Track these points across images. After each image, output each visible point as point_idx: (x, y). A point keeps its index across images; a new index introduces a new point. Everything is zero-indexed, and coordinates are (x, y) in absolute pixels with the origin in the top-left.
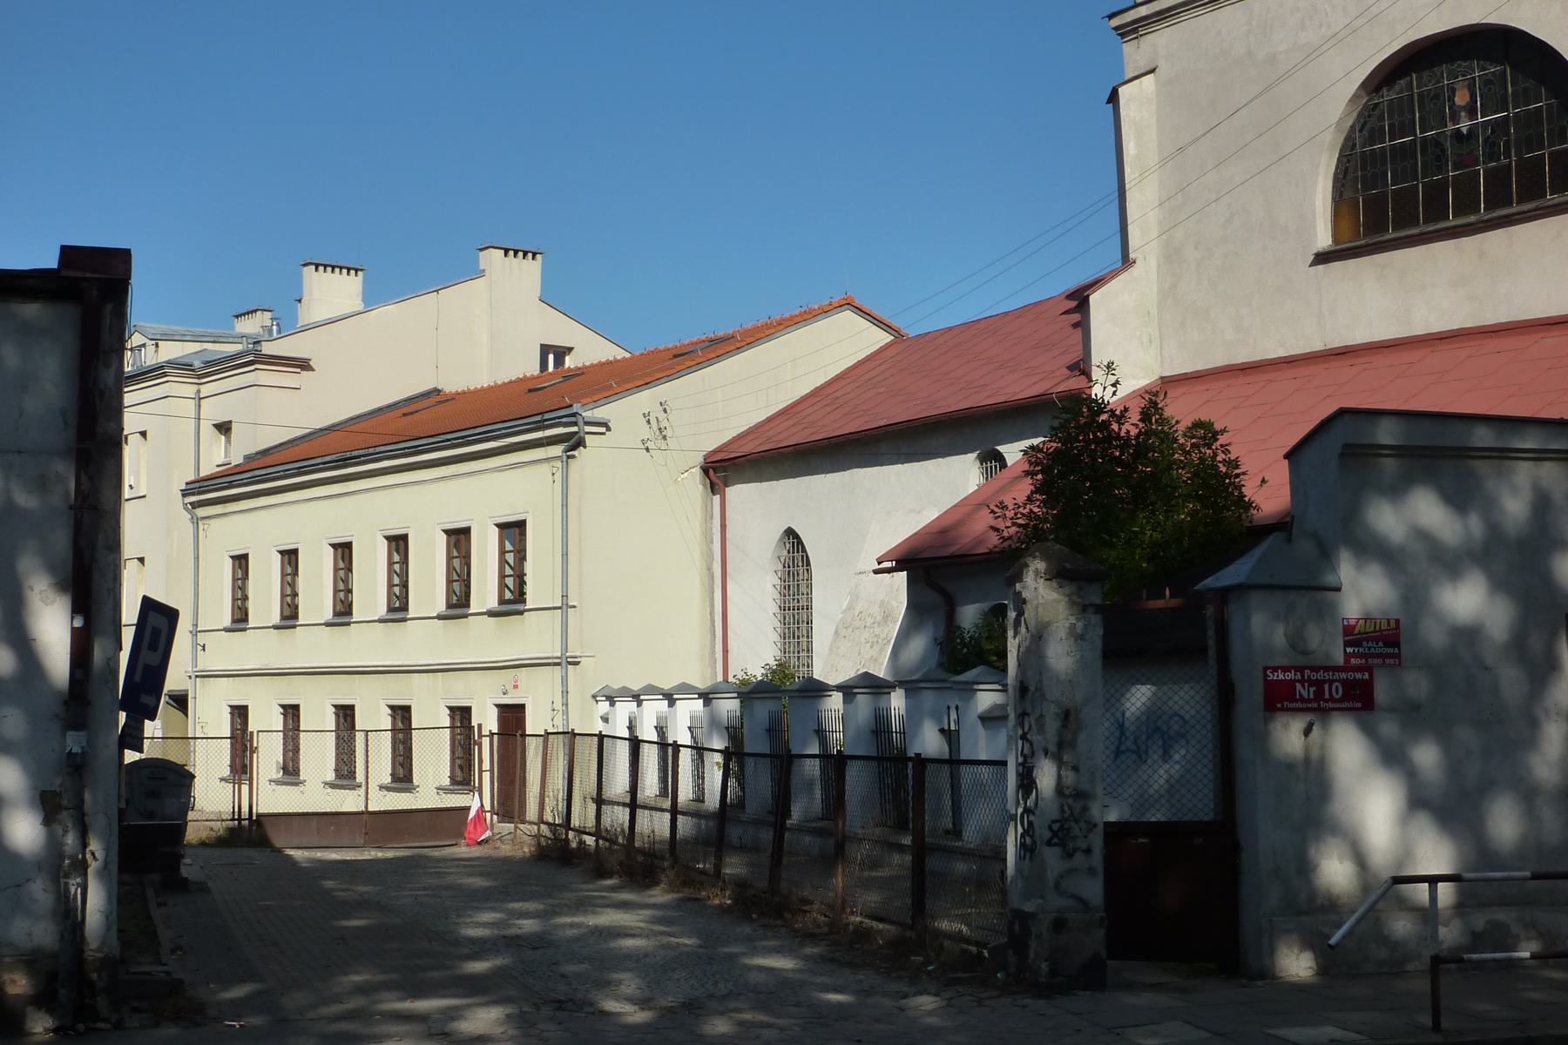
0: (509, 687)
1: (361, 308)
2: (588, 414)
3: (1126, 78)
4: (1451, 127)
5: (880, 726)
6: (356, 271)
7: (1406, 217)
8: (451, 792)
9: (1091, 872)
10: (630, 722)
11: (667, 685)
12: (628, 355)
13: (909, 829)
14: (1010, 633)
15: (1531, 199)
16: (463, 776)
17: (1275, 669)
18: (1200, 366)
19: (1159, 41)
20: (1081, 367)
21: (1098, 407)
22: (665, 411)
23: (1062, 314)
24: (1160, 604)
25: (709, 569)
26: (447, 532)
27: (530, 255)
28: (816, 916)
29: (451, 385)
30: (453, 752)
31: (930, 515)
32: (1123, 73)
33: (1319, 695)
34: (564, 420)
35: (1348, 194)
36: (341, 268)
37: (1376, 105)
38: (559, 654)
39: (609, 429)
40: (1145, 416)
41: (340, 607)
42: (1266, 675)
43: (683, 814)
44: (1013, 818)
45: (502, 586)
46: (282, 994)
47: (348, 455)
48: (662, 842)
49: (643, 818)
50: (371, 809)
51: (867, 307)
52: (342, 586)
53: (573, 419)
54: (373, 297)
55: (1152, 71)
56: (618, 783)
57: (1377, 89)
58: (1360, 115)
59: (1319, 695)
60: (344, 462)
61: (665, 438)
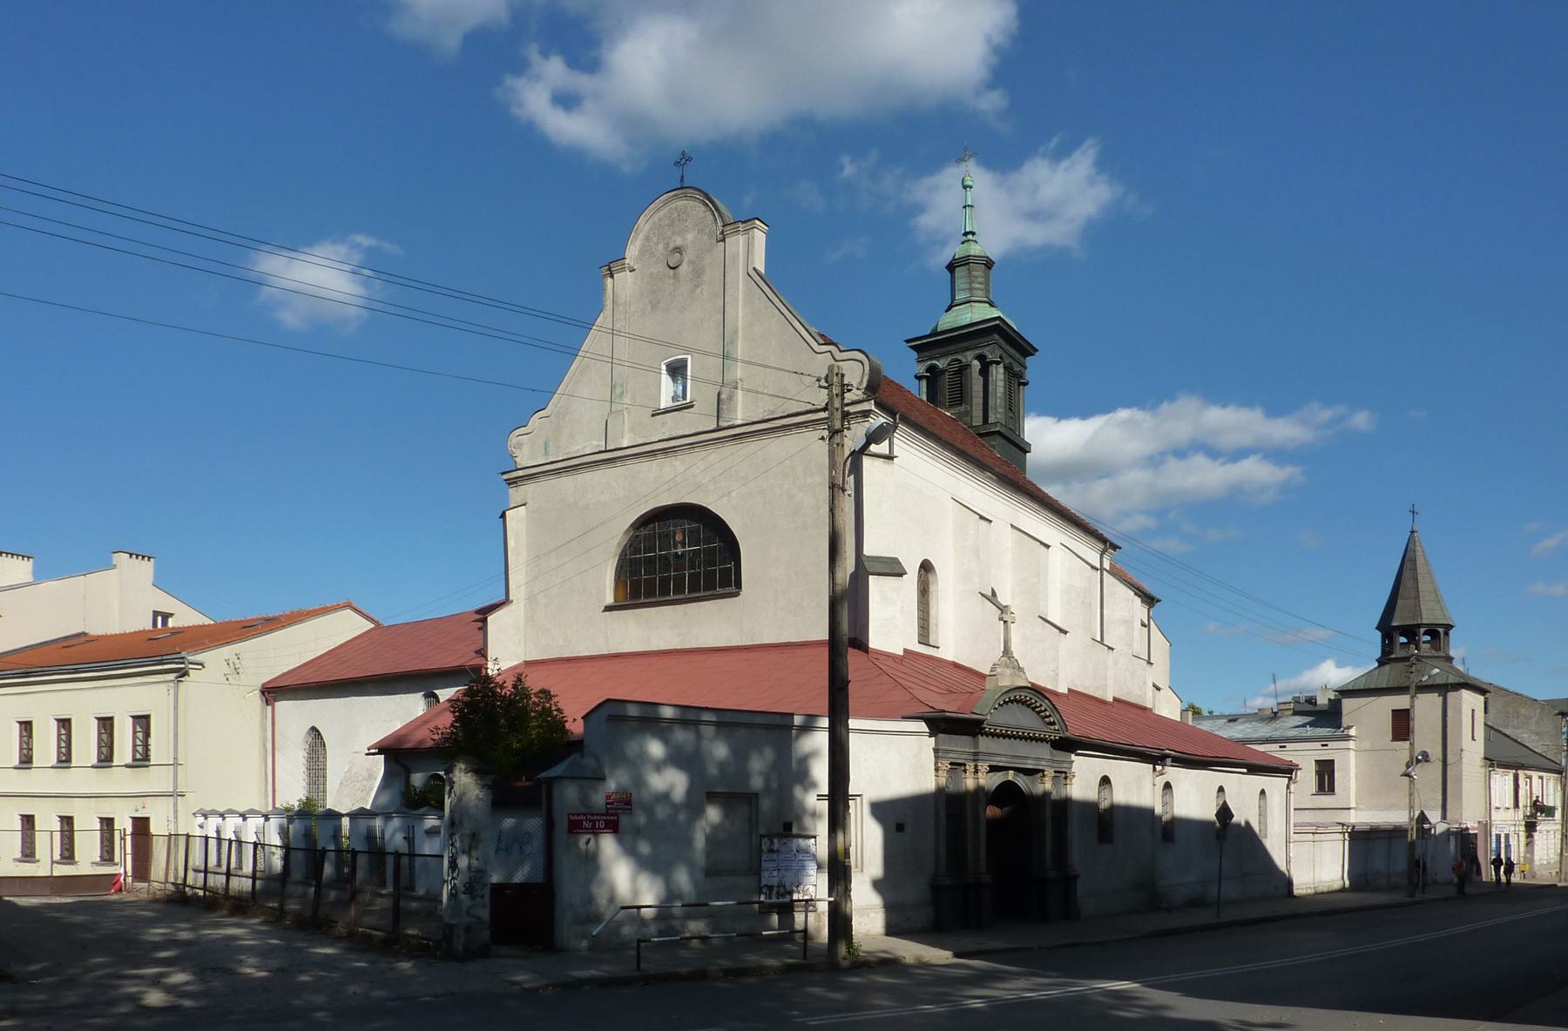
0: (140, 808)
1: (30, 578)
2: (191, 658)
3: (511, 507)
4: (673, 551)
5: (370, 836)
6: (28, 558)
7: (650, 593)
8: (102, 865)
9: (484, 906)
10: (217, 828)
11: (241, 810)
12: (212, 623)
13: (880, 810)
14: (446, 797)
15: (709, 590)
16: (107, 855)
17: (573, 815)
18: (545, 657)
19: (527, 490)
20: (483, 652)
21: (488, 679)
22: (238, 658)
23: (474, 621)
24: (519, 784)
25: (265, 746)
26: (98, 719)
27: (146, 558)
28: (341, 929)
29: (94, 630)
30: (102, 843)
31: (397, 725)
32: (508, 503)
33: (594, 827)
34: (176, 660)
35: (622, 578)
36: (18, 555)
37: (637, 536)
38: (172, 790)
39: (204, 667)
40: (515, 687)
41: (24, 758)
42: (569, 818)
43: (259, 879)
44: (445, 881)
45: (135, 751)
46: (482, 877)
47: (30, 670)
48: (248, 892)
49: (211, 878)
50: (54, 874)
51: (359, 608)
52: (25, 746)
53: (182, 660)
54: (40, 575)
55: (524, 505)
56: (197, 859)
57: (638, 528)
58: (629, 541)
59: (594, 827)
60: (27, 675)
61: (238, 673)
